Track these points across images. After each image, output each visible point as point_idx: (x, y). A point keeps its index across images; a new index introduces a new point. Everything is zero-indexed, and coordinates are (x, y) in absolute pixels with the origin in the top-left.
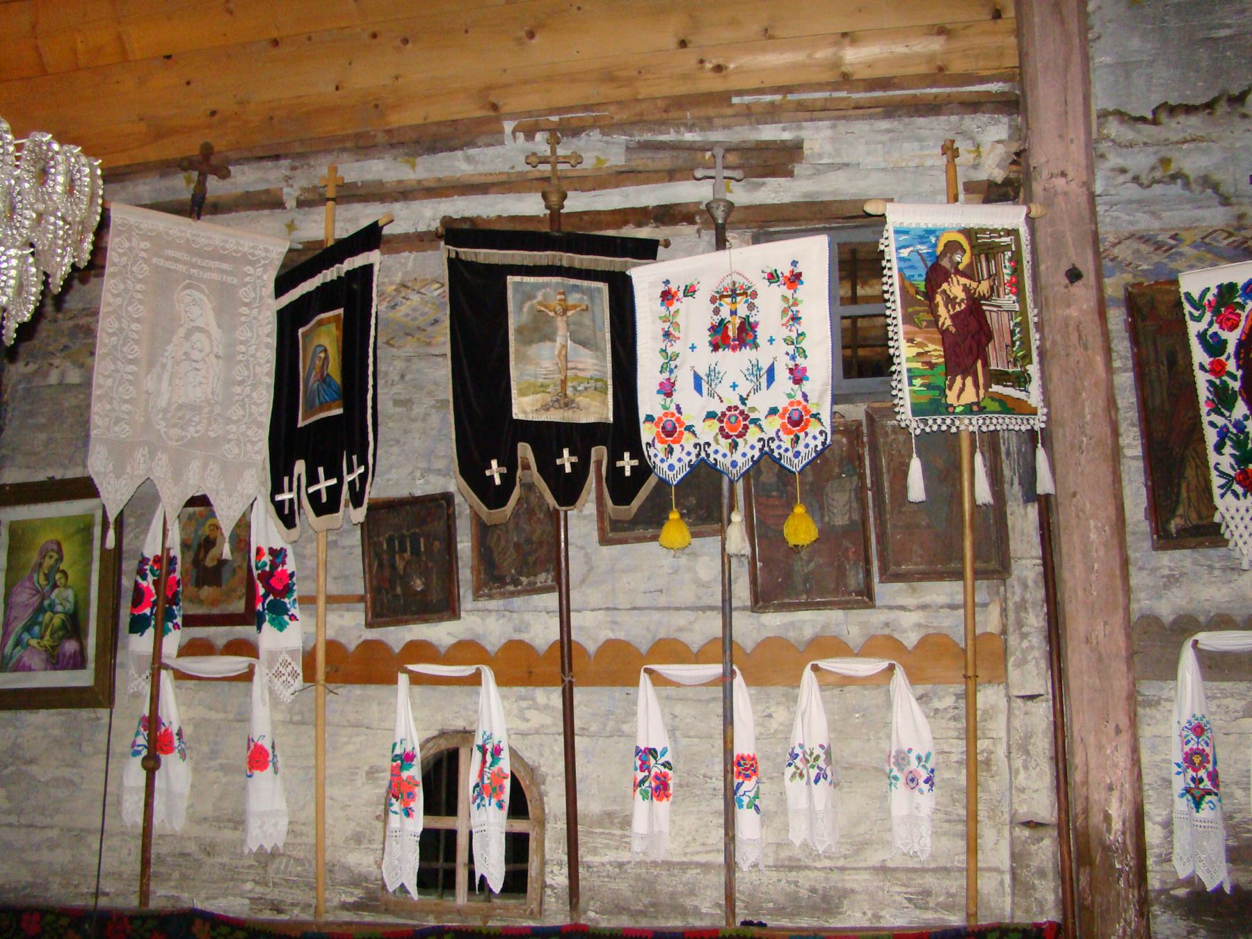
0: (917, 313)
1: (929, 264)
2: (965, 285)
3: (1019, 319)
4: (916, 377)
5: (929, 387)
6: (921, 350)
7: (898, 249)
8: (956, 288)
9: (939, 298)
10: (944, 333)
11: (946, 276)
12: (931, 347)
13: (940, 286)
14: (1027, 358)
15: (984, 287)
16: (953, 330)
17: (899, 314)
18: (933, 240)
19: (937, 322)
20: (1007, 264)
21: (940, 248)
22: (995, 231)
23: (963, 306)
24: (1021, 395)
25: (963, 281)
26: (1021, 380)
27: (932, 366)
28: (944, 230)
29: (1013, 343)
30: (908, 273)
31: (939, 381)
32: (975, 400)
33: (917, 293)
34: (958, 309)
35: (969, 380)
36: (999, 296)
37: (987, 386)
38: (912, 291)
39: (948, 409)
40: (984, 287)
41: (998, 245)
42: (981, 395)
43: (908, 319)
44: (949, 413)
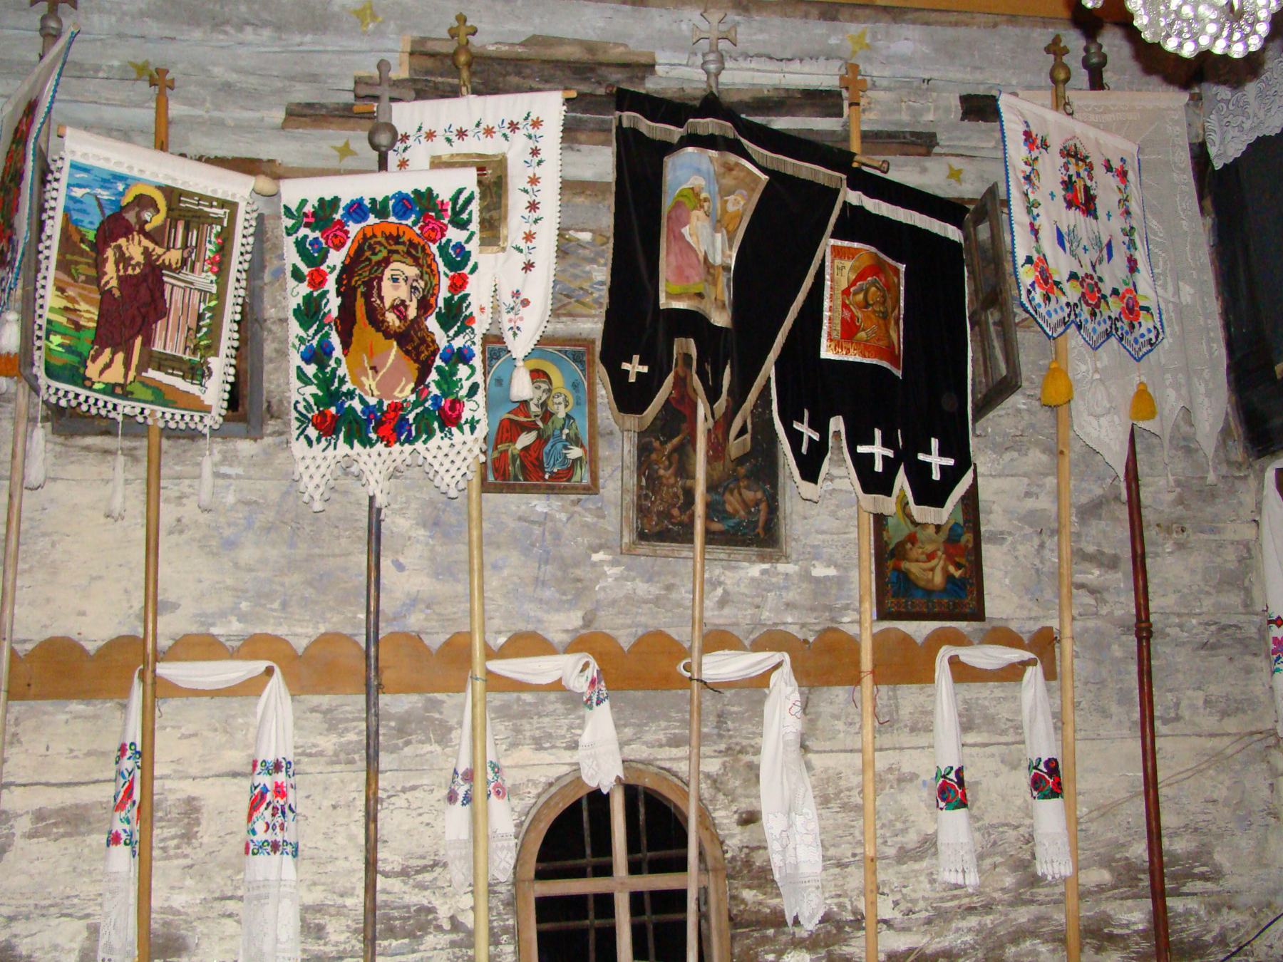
0: (77, 263)
1: (108, 213)
2: (146, 249)
3: (213, 303)
4: (56, 333)
5: (69, 349)
6: (70, 305)
7: (69, 186)
8: (135, 249)
9: (110, 253)
10: (106, 294)
11: (127, 231)
12: (83, 306)
13: (115, 240)
14: (213, 349)
15: (174, 256)
16: (117, 293)
17: (54, 254)
18: (121, 187)
19: (99, 279)
20: (213, 239)
21: (129, 198)
22: (202, 197)
23: (138, 271)
24: (194, 389)
25: (146, 243)
26: (197, 372)
27: (78, 327)
28: (137, 180)
29: (199, 329)
30: (75, 216)
31: (85, 347)
32: (121, 381)
33: (83, 240)
34: (130, 271)
35: (120, 357)
36: (193, 270)
37: (142, 367)
38: (76, 238)
39: (84, 382)
40: (174, 256)
41: (207, 215)
42: (131, 378)
43: (63, 265)
44: (84, 387)
